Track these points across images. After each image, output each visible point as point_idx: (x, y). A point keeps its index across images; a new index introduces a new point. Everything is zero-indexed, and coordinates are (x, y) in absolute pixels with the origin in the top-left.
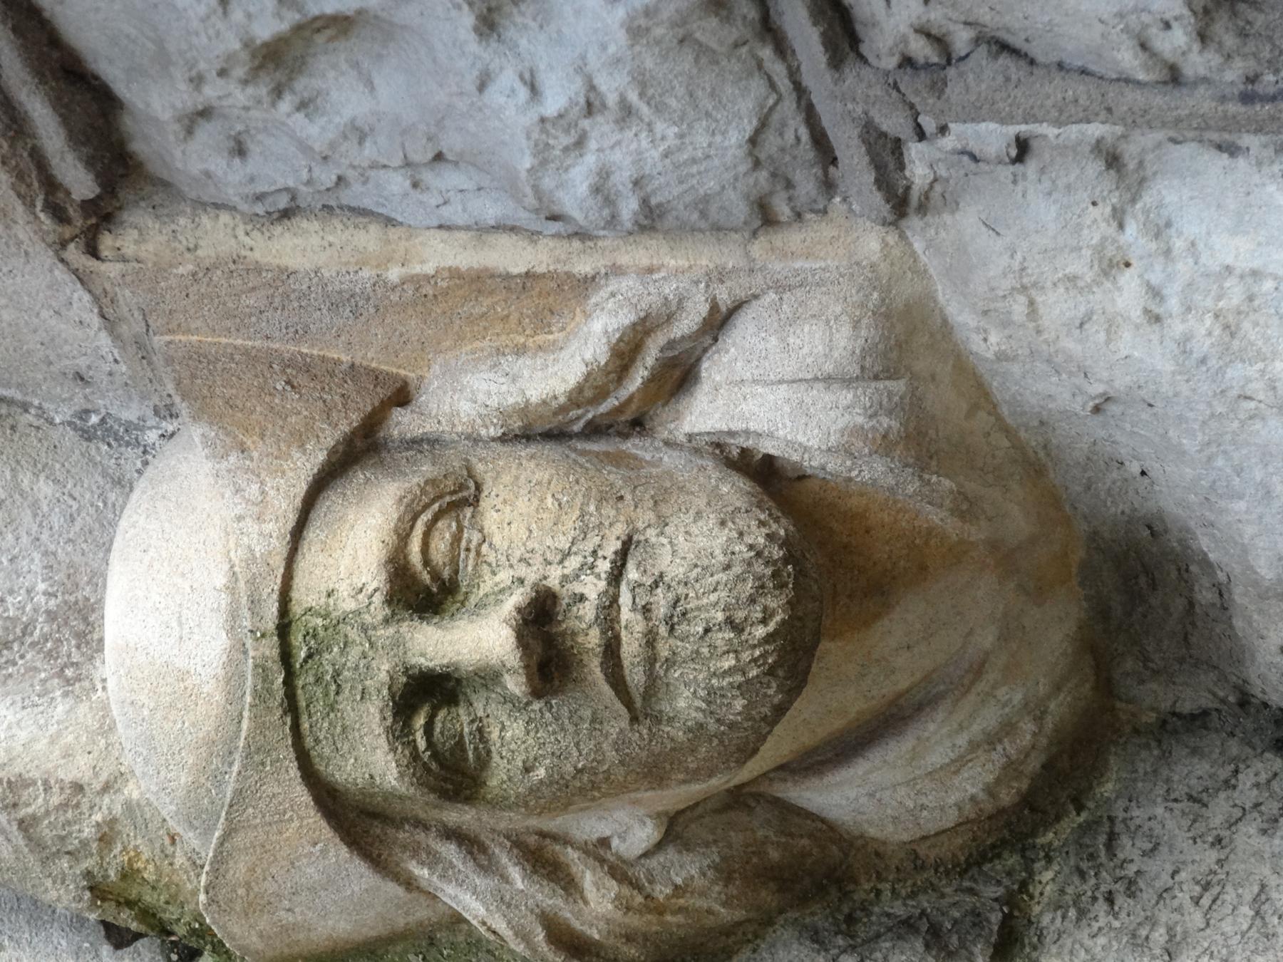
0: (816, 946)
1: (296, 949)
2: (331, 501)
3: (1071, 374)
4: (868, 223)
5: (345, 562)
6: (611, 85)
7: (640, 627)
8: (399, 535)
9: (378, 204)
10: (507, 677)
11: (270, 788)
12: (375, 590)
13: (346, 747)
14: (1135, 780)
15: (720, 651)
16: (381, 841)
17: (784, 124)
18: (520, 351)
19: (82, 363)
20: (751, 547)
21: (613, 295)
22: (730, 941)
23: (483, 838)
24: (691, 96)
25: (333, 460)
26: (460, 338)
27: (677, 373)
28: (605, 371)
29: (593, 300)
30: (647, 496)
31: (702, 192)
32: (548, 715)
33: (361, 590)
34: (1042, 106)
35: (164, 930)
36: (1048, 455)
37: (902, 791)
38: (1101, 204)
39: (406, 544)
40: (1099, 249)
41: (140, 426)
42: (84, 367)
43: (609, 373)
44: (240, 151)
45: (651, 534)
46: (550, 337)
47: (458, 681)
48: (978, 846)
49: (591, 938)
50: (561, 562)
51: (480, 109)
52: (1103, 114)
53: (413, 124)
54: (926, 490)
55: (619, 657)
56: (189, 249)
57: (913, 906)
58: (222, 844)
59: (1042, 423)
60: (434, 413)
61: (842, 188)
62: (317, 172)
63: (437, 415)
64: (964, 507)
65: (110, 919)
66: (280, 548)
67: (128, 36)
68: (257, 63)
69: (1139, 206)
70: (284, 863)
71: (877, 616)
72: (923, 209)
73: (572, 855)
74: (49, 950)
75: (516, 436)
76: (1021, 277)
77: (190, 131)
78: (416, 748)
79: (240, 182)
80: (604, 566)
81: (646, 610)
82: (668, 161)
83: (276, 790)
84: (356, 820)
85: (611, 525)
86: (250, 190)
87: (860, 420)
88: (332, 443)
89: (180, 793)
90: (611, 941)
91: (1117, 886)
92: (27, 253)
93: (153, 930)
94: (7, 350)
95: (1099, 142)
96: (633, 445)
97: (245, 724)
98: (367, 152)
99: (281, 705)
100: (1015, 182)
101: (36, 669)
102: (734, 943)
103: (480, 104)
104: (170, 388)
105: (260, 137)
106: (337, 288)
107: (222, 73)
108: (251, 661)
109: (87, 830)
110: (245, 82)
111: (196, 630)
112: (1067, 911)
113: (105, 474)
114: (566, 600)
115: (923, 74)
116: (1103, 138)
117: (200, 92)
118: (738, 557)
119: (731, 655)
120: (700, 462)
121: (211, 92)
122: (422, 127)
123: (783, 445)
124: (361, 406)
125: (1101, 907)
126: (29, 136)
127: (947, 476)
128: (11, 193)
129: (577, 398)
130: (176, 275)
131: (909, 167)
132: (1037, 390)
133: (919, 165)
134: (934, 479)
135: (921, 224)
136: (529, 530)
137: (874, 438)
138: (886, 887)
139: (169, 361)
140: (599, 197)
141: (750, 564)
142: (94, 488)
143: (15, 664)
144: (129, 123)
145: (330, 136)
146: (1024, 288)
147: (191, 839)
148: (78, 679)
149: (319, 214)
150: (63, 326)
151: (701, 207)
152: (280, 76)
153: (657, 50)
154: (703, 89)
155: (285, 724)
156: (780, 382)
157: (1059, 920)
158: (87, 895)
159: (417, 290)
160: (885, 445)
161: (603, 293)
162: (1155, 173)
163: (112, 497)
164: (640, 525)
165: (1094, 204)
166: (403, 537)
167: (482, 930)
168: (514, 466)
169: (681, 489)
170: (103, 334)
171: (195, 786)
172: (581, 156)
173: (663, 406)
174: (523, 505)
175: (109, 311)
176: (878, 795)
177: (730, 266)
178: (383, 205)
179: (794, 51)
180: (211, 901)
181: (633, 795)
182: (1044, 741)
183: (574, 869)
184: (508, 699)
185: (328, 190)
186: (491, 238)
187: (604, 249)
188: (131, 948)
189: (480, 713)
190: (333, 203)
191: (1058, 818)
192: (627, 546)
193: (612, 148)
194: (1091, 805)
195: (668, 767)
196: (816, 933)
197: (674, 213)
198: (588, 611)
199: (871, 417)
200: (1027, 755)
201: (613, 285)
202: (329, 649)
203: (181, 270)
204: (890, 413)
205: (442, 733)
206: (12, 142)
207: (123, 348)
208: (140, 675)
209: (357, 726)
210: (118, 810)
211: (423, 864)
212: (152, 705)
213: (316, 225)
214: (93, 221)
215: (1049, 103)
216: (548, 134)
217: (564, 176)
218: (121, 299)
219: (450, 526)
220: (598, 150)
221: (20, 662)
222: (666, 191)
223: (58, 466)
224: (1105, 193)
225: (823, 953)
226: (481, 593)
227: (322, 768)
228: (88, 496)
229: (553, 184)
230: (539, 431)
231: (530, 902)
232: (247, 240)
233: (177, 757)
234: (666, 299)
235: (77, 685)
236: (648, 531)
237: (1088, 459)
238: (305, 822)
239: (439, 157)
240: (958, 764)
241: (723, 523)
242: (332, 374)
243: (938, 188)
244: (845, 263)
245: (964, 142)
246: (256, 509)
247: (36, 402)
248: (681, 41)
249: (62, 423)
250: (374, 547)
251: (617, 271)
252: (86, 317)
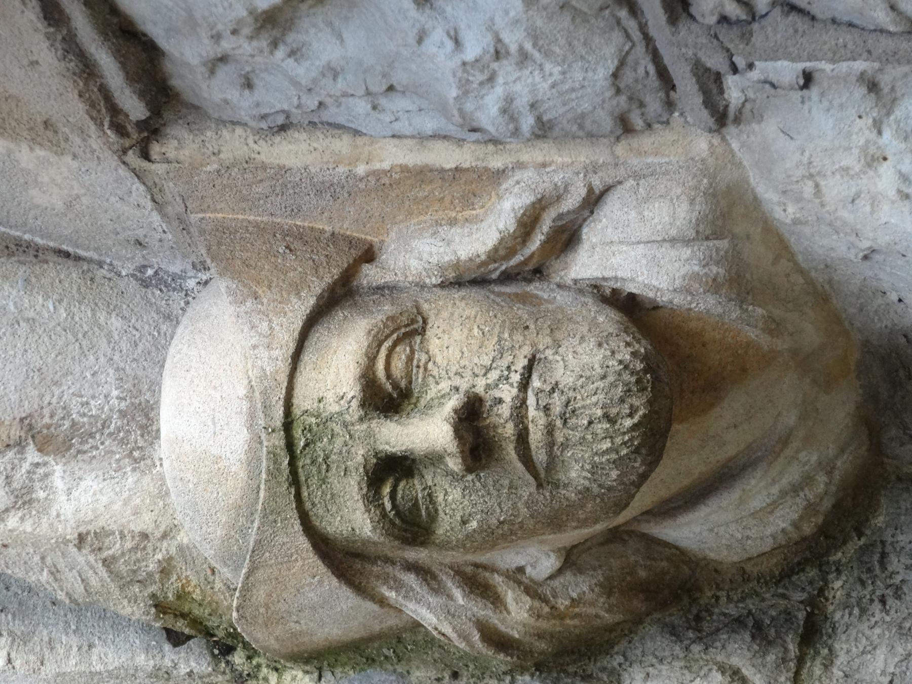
0: (674, 638)
1: (303, 648)
2: (320, 334)
3: (846, 234)
4: (699, 131)
5: (331, 377)
6: (513, 39)
7: (542, 421)
8: (369, 358)
9: (348, 120)
10: (448, 459)
11: (281, 539)
12: (353, 398)
13: (334, 509)
14: (899, 515)
15: (600, 437)
16: (361, 574)
17: (637, 63)
18: (453, 222)
19: (140, 233)
20: (621, 362)
21: (518, 183)
22: (612, 636)
23: (433, 569)
24: (570, 45)
25: (321, 303)
26: (410, 213)
27: (565, 236)
28: (514, 236)
29: (504, 186)
30: (546, 326)
31: (579, 111)
32: (478, 484)
33: (342, 398)
34: (821, 50)
35: (208, 633)
36: (832, 287)
37: (733, 527)
38: (864, 118)
40: (864, 149)
41: (183, 277)
42: (141, 236)
43: (516, 238)
44: (249, 85)
45: (549, 353)
46: (474, 212)
47: (414, 460)
48: (788, 563)
49: (512, 637)
50: (485, 375)
51: (419, 56)
52: (865, 55)
53: (372, 66)
54: (744, 316)
55: (528, 443)
56: (214, 154)
57: (743, 608)
58: (247, 578)
59: (827, 266)
60: (392, 267)
61: (680, 106)
62: (304, 99)
63: (394, 270)
64: (773, 327)
65: (170, 626)
66: (284, 368)
67: (166, 6)
68: (259, 25)
69: (892, 118)
70: (293, 590)
71: (712, 405)
72: (737, 120)
73: (498, 579)
74: (127, 647)
75: (451, 283)
76: (809, 168)
77: (212, 72)
78: (384, 509)
79: (250, 107)
80: (516, 378)
81: (547, 409)
82: (554, 91)
83: (285, 540)
84: (342, 559)
85: (520, 347)
86: (255, 112)
87: (696, 268)
88: (320, 291)
89: (217, 542)
90: (527, 639)
91: (888, 591)
92: (98, 158)
93: (200, 633)
94: (86, 225)
95: (862, 74)
96: (535, 287)
97: (262, 494)
98: (339, 86)
99: (287, 480)
100: (803, 102)
101: (113, 452)
102: (616, 637)
103: (419, 52)
104: (204, 251)
105: (262, 75)
106: (321, 180)
107: (234, 32)
108: (265, 449)
109: (152, 566)
110: (251, 38)
111: (225, 427)
112: (852, 609)
113: (158, 312)
114: (489, 403)
115: (735, 28)
117: (219, 45)
118: (611, 370)
119: (608, 440)
120: (583, 299)
121: (227, 44)
122: (379, 68)
123: (642, 286)
124: (340, 263)
125: (877, 607)
126: (98, 77)
127: (760, 306)
128: (87, 116)
129: (494, 256)
130: (205, 172)
132: (822, 244)
133: (734, 91)
134: (751, 308)
135: (737, 130)
136: (461, 352)
137: (707, 282)
138: (723, 594)
139: (202, 232)
140: (506, 116)
141: (620, 375)
142: (151, 322)
143: (97, 449)
145: (313, 74)
146: (811, 176)
147: (225, 572)
148: (143, 458)
149: (307, 128)
150: (126, 208)
151: (579, 121)
152: (276, 33)
153: (544, 14)
154: (579, 40)
155: (290, 493)
156: (639, 243)
157: (847, 616)
158: (153, 610)
159: (378, 180)
160: (715, 286)
161: (511, 182)
162: (903, 95)
163: (164, 328)
164: (541, 347)
165: (860, 117)
166: (372, 359)
167: (435, 633)
168: (450, 305)
169: (570, 320)
170: (155, 213)
171: (228, 537)
172: (492, 87)
173: (556, 259)
174: (457, 334)
175: (158, 197)
176: (716, 530)
177: (601, 161)
178: (352, 122)
179: (642, 12)
180: (241, 617)
181: (540, 538)
182: (833, 489)
183: (499, 589)
184: (448, 473)
185: (312, 111)
186: (430, 144)
187: (510, 151)
188: (186, 646)
189: (430, 483)
190: (316, 120)
191: (845, 542)
192: (529, 370)
193: (514, 82)
194: (868, 532)
195: (565, 518)
196: (674, 628)
197: (560, 126)
198: (505, 410)
199: (704, 266)
200: (821, 499)
201: (518, 175)
202: (320, 439)
203: (209, 168)
204: (717, 263)
205: (403, 498)
206: (86, 82)
207: (169, 223)
208: (186, 460)
209: (342, 494)
210: (173, 551)
211: (391, 588)
212: (195, 481)
213: (304, 136)
214: (146, 134)
215: (826, 47)
216: (468, 73)
217: (481, 102)
218: (166, 189)
219: (405, 350)
220: (504, 83)
221: (101, 447)
222: (553, 111)
223: (125, 306)
224: (868, 110)
225: (679, 643)
226: (429, 397)
227: (318, 524)
228: (147, 327)
229: (473, 107)
230: (468, 279)
231: (469, 613)
233: (214, 517)
234: (556, 185)
235: (142, 463)
236: (547, 351)
237: (861, 290)
238: (306, 562)
239: (391, 88)
240: (773, 507)
241: (600, 345)
242: (318, 240)
243: (748, 106)
244: (683, 158)
245: (766, 75)
246: (266, 340)
247: (108, 261)
248: (562, 7)
249: (127, 275)
250: (351, 367)
251: (520, 165)
252: (142, 201)
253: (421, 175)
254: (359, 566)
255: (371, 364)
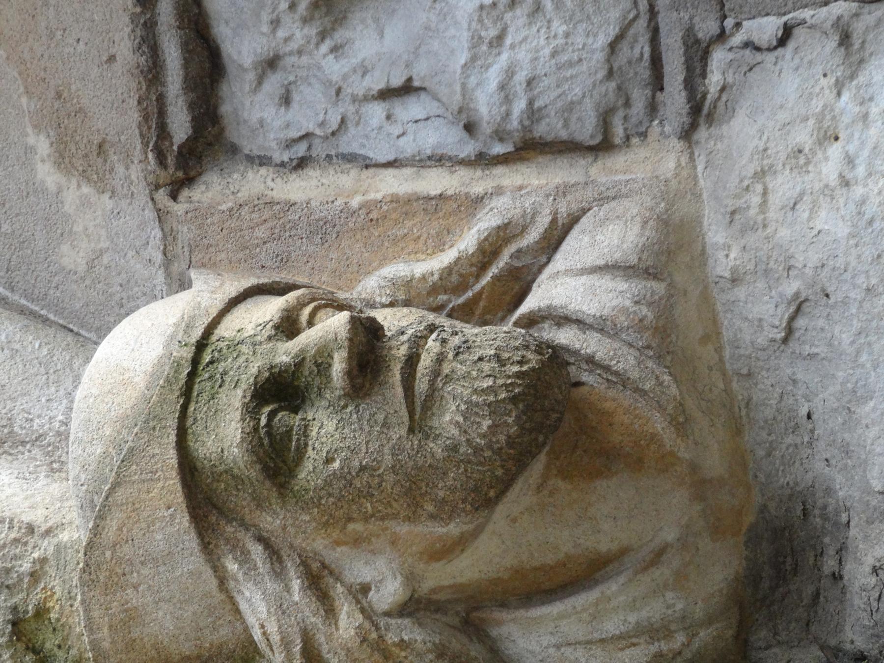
15: (484, 374)
23: (282, 553)
38: (829, 76)
39: (301, 309)
78: (258, 423)
83: (157, 451)
84: (204, 496)
87: (628, 303)
99: (181, 389)
116: (842, 16)
119: (491, 378)
131: (709, 76)
137: (634, 320)
144: (224, 89)
148: (60, 470)
149: (322, 163)
151: (566, 115)
159: (367, 214)
162: (871, 54)
165: (825, 75)
183: (337, 603)
187: (495, 176)
204: (650, 304)
205: (280, 421)
231: (299, 615)
232: (270, 184)
234: (525, 211)
251: (499, 191)
253: (405, 205)
254: (214, 518)
255: (299, 307)
